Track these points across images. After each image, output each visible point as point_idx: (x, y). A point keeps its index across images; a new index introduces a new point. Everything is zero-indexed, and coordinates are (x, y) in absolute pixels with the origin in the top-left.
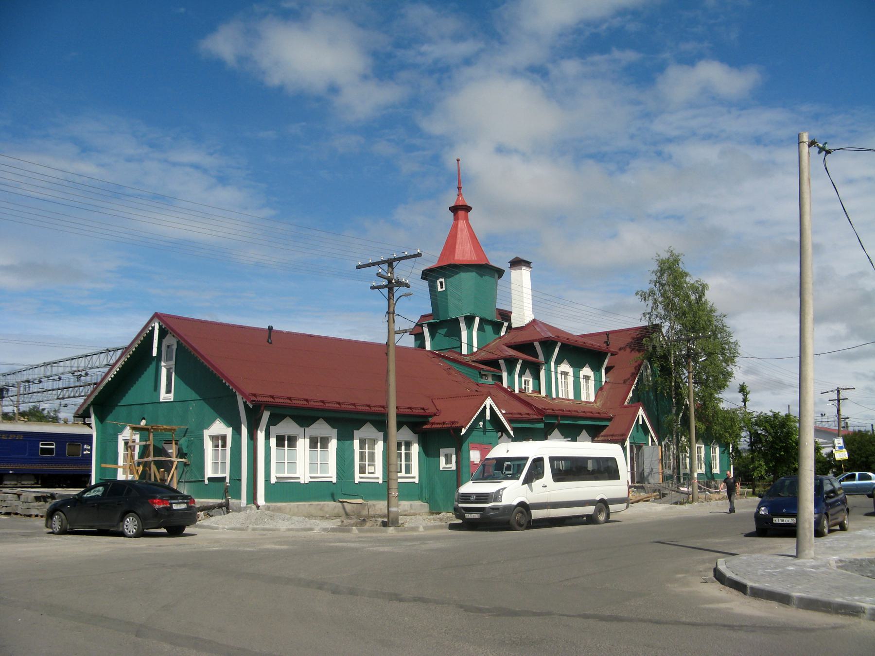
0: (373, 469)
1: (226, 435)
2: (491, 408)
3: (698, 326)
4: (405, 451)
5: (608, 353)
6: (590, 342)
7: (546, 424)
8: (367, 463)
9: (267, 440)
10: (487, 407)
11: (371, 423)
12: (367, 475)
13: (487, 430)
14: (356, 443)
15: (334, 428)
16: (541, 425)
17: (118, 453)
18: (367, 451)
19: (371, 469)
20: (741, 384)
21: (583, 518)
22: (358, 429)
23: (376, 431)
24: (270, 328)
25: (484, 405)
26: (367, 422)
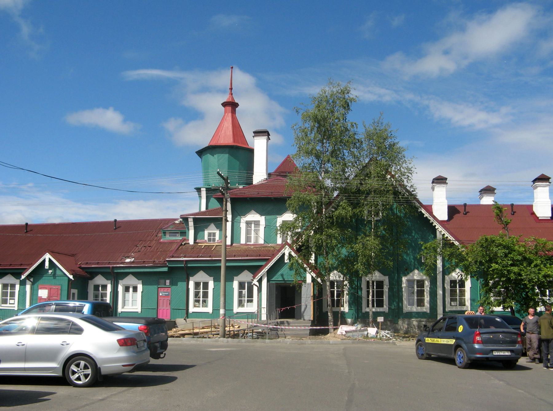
1: (208, 307)
2: (50, 260)
3: (375, 125)
6: (436, 178)
7: (169, 268)
8: (9, 298)
9: (22, 287)
10: (46, 260)
11: (132, 274)
12: (8, 305)
13: (56, 276)
14: (236, 284)
15: (210, 276)
16: (165, 269)
18: (201, 290)
19: (12, 301)
20: (495, 191)
21: (416, 335)
22: (237, 276)
23: (15, 279)
24: (27, 224)
25: (280, 255)
26: (98, 275)
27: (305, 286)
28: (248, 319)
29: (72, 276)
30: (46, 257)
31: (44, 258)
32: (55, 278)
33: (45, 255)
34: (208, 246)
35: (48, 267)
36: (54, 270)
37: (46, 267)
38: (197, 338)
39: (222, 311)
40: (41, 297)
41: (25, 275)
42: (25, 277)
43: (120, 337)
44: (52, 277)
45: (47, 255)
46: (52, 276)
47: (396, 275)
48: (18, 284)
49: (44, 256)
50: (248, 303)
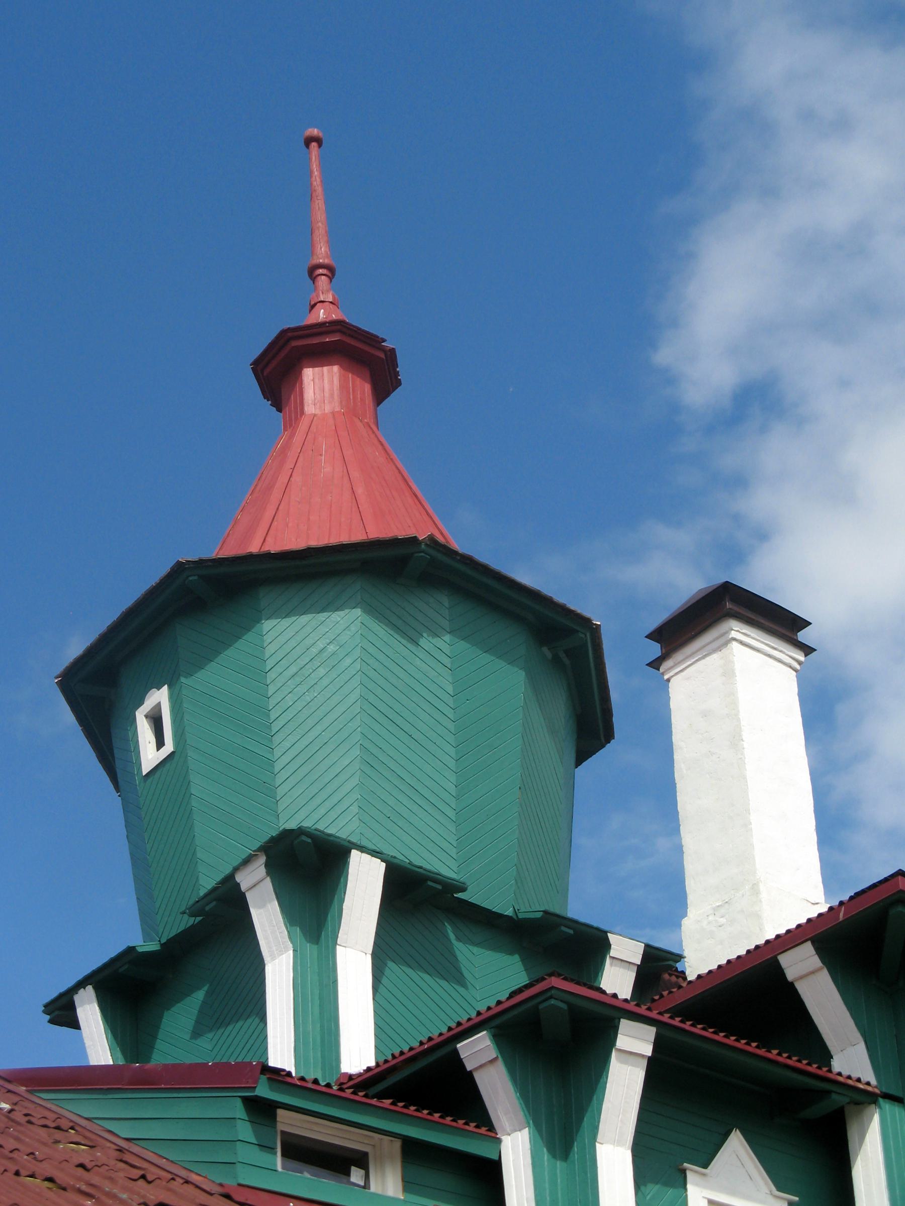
5: (806, 655)
17: (802, 716)
28: (261, 1021)
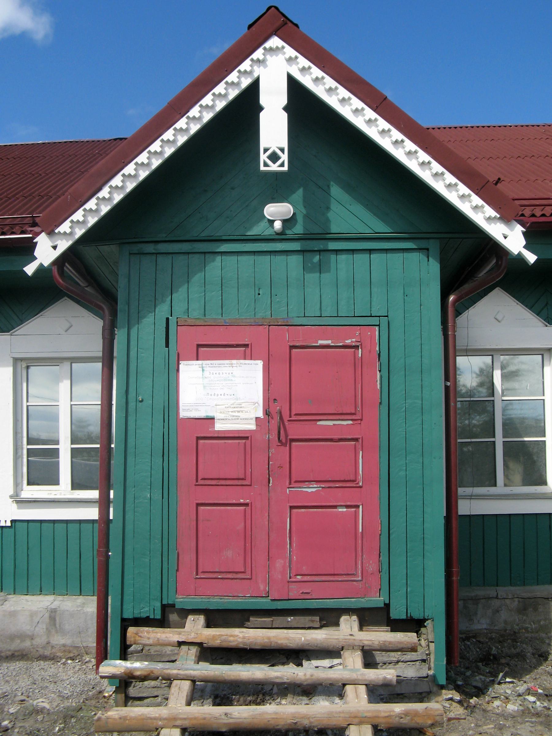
0: (490, 362)
4: (494, 442)
10: (306, 81)
27: (434, 458)
28: (287, 256)
29: (519, 229)
30: (258, 71)
31: (246, 82)
32: (321, 268)
33: (258, 54)
34: (125, 163)
35: (284, 157)
36: (307, 202)
37: (263, 157)
38: (401, 676)
39: (7, 701)
40: (211, 420)
41: (65, 227)
42: (64, 245)
43: (348, 668)
44: (295, 261)
45: (271, 60)
46: (296, 246)
47: (361, 452)
48: (497, 369)
49: (246, 65)
50: (149, 615)
